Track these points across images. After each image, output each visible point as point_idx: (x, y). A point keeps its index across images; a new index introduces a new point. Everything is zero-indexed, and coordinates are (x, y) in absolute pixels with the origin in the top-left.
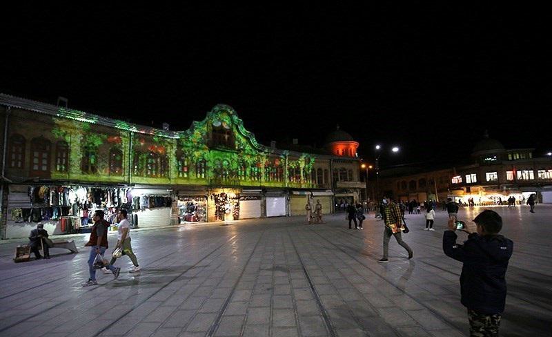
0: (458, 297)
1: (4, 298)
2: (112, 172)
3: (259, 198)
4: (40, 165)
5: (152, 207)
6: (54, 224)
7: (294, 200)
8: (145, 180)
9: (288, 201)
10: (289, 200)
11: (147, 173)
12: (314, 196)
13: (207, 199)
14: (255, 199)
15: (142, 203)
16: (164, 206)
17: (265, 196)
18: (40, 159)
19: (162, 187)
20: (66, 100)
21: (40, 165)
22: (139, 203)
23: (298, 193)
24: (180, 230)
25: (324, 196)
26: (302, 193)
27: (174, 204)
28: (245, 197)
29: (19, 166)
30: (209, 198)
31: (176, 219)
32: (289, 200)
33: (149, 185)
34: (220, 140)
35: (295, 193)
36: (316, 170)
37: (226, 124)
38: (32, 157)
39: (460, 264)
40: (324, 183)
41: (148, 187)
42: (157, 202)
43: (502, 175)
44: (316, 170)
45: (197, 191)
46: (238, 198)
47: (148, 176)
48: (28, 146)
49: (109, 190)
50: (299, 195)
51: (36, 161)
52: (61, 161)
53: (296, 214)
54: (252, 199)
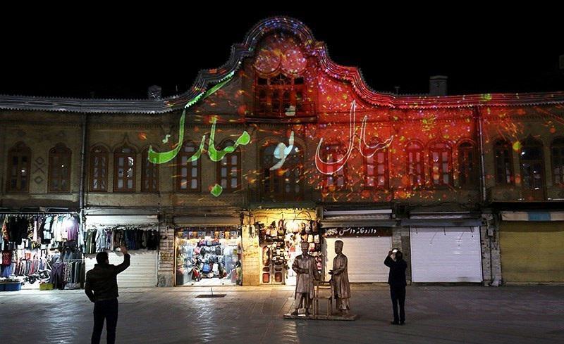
2: (53, 189)
3: (383, 231)
7: (511, 240)
8: (111, 199)
9: (488, 242)
11: (115, 183)
13: (240, 234)
17: (408, 228)
22: (94, 242)
23: (523, 216)
24: (284, 339)
26: (542, 217)
28: (339, 229)
30: (246, 233)
32: (492, 239)
33: (120, 207)
34: (271, 107)
35: (508, 216)
37: (293, 61)
39: (110, 263)
41: (114, 211)
43: (310, 95)
46: (319, 230)
47: (116, 191)
49: (37, 220)
53: (523, 279)
54: (361, 235)
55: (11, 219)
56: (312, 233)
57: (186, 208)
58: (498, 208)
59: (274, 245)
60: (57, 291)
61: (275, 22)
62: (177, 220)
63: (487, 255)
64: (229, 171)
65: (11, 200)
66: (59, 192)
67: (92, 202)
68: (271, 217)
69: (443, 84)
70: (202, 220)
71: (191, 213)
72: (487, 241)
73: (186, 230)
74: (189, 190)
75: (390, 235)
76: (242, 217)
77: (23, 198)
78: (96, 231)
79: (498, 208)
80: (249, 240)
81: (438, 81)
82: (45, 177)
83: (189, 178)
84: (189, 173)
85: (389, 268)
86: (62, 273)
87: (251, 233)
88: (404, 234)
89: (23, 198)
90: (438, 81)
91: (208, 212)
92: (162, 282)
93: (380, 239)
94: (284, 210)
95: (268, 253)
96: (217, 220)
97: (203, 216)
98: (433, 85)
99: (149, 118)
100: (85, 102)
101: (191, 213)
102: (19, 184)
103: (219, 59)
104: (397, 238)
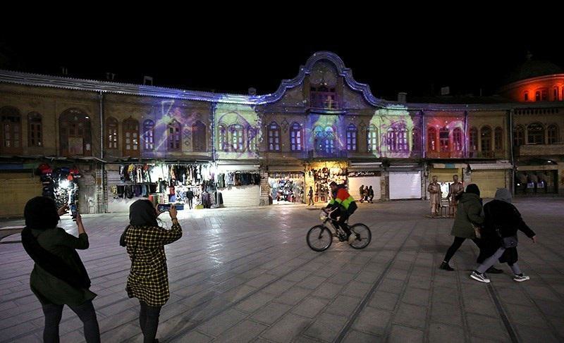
3: (377, 173)
5: (239, 185)
10: (427, 177)
12: (474, 171)
13: (304, 175)
15: (227, 180)
16: (252, 184)
17: (388, 172)
19: (250, 163)
20: (150, 79)
22: (224, 181)
23: (443, 166)
26: (451, 166)
27: (263, 181)
30: (307, 175)
31: (266, 198)
32: (427, 177)
35: (436, 166)
40: (493, 149)
41: (234, 162)
42: (244, 180)
46: (346, 173)
48: (120, 128)
51: (128, 141)
54: (366, 176)
55: (176, 167)
56: (343, 175)
57: (274, 161)
58: (430, 162)
59: (322, 182)
60: (206, 209)
61: (329, 55)
62: (270, 168)
63: (424, 185)
64: (238, 141)
65: (171, 155)
66: (199, 151)
67: (220, 158)
68: (320, 166)
69: (404, 97)
70: (284, 168)
71: (277, 164)
72: (424, 178)
73: (275, 173)
74: (274, 151)
75: (380, 175)
76: (305, 165)
77: (179, 154)
78: (224, 175)
79: (430, 162)
80: (309, 180)
81: (402, 95)
82: (191, 141)
83: (274, 144)
84: (274, 141)
85: (33, 262)
86: (209, 198)
87: (310, 175)
88: (387, 175)
89: (179, 154)
90: (402, 95)
91: (286, 163)
92: (262, 203)
93: (375, 177)
94: (327, 162)
95: (317, 186)
96: (291, 168)
97: (283, 166)
98: (399, 97)
99: (64, 92)
100: (206, 94)
101: (277, 164)
102: (175, 146)
103: (293, 73)
104: (383, 177)
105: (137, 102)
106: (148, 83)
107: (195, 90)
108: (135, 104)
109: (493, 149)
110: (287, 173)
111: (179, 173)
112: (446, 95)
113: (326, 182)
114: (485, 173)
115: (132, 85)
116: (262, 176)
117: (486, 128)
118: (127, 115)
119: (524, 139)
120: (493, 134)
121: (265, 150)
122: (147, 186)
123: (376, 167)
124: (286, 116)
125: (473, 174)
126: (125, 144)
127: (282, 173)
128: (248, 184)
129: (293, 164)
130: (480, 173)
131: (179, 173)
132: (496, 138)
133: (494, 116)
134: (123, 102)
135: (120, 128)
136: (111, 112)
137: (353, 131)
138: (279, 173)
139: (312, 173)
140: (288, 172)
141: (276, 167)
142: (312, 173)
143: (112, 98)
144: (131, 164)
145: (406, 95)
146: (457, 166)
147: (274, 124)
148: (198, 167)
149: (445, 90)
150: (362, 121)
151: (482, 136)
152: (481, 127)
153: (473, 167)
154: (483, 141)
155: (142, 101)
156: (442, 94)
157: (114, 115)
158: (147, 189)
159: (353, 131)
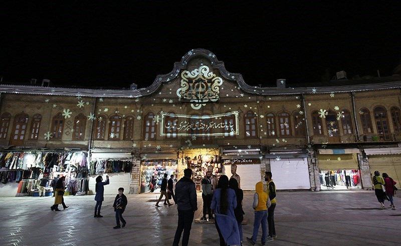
0: (277, 223)
1: (116, 235)
3: (256, 161)
4: (19, 135)
6: (14, 187)
12: (369, 156)
13: (177, 163)
14: (249, 163)
15: (99, 167)
18: (20, 130)
20: (48, 81)
21: (19, 135)
22: (95, 168)
23: (330, 152)
25: (388, 156)
27: (135, 169)
29: (4, 137)
30: (180, 162)
32: (314, 164)
35: (322, 152)
36: (371, 110)
38: (14, 129)
40: (392, 130)
44: (371, 110)
45: (165, 153)
48: (12, 120)
50: (262, 224)
51: (17, 132)
52: (35, 131)
54: (243, 163)
55: (49, 155)
60: (72, 197)
62: (142, 156)
66: (78, 140)
68: (194, 153)
70: (156, 155)
76: (178, 154)
77: (58, 143)
87: (183, 162)
89: (58, 143)
93: (254, 165)
105: (31, 100)
106: (46, 85)
107: (76, 88)
108: (28, 101)
109: (392, 130)
110: (160, 161)
111: (51, 161)
112: (342, 79)
113: (200, 170)
114: (386, 159)
115: (24, 87)
116: (134, 164)
117: (378, 109)
118: (20, 110)
119: (388, 120)
120: (389, 114)
121: (140, 138)
122: (22, 172)
123: (255, 153)
124: (162, 107)
125: (371, 160)
126: (13, 135)
127: (156, 161)
128: (119, 172)
129: (168, 151)
130: (380, 160)
131: (51, 161)
132: (394, 119)
133: (385, 96)
134: (19, 100)
135: (12, 120)
136: (7, 108)
137: (286, 117)
138: (151, 161)
139: (184, 161)
140: (162, 160)
141: (280, 148)
142: (184, 161)
143: (11, 97)
144: (10, 152)
145: (288, 84)
146: (347, 151)
147: (151, 114)
148: (70, 155)
149: (341, 74)
150: (239, 107)
151: (376, 118)
152: (373, 107)
153: (368, 152)
154: (378, 123)
155: (35, 98)
156: (338, 78)
157: (9, 110)
158: (21, 175)
159: (286, 117)
